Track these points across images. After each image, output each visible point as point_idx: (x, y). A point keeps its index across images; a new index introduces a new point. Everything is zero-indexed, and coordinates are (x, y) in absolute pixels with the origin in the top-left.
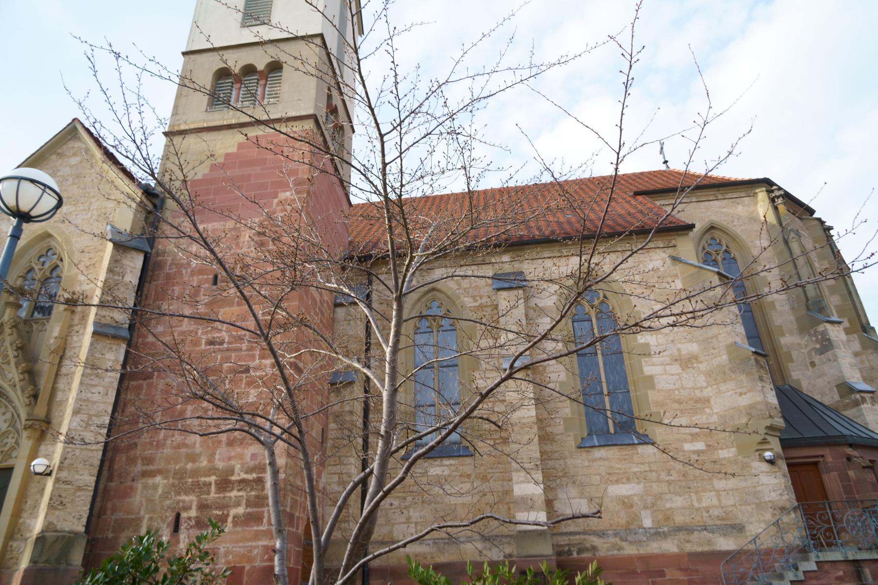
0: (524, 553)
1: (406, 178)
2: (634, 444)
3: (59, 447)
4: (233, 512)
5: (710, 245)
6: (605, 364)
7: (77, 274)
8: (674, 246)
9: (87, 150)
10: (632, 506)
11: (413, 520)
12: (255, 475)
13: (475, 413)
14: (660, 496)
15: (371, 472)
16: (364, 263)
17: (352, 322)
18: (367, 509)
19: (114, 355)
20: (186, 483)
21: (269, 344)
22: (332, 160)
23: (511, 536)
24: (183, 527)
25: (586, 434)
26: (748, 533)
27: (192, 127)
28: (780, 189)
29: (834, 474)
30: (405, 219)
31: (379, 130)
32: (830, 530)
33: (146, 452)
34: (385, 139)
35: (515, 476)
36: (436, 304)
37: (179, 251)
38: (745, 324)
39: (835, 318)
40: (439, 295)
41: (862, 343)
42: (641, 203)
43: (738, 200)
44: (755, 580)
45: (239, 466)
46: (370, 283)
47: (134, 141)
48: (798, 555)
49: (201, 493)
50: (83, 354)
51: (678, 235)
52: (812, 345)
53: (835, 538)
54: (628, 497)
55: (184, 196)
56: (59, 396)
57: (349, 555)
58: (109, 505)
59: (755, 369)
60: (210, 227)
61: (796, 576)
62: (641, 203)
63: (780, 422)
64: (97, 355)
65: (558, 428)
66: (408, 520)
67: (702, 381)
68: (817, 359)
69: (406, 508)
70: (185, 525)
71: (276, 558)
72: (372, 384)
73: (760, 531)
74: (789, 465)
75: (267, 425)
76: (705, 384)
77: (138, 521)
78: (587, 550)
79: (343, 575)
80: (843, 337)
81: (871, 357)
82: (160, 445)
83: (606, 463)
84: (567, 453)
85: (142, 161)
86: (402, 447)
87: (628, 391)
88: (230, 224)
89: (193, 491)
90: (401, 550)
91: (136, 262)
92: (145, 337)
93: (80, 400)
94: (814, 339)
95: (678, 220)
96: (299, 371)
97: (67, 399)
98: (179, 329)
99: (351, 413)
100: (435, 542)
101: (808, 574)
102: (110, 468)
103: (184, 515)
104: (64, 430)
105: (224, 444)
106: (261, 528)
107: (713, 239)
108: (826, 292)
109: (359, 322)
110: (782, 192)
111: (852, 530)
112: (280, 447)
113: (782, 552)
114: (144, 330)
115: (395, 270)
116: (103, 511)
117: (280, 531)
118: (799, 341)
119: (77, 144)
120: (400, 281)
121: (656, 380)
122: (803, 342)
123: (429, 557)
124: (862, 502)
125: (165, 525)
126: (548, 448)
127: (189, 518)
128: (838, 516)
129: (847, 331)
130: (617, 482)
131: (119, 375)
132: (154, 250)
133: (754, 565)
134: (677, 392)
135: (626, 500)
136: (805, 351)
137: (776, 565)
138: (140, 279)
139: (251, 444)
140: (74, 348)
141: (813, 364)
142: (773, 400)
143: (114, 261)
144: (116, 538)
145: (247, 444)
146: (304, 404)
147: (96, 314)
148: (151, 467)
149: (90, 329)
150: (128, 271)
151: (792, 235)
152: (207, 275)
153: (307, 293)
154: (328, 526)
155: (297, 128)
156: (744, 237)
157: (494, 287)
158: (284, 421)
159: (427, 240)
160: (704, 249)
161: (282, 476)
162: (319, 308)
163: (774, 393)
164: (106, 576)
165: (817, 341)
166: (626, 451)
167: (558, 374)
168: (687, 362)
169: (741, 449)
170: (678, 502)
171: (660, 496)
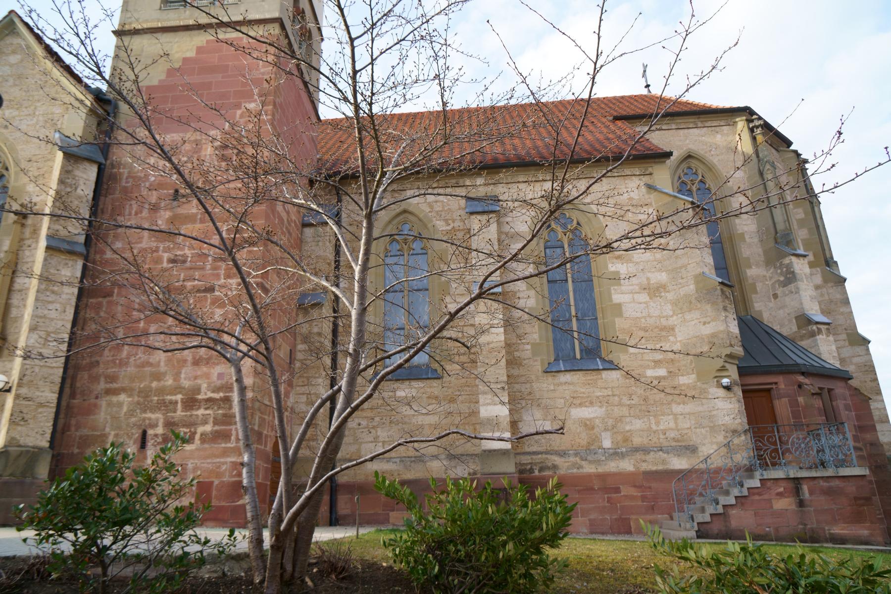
0: (486, 471)
1: (377, 86)
2: (598, 370)
3: (18, 361)
4: (200, 429)
5: (686, 174)
6: (575, 291)
7: (25, 185)
8: (651, 174)
9: (28, 47)
10: (593, 428)
11: (381, 439)
12: (222, 394)
13: (445, 333)
14: (619, 420)
15: (339, 390)
16: (335, 182)
17: (320, 244)
18: (335, 424)
19: (72, 270)
20: (151, 401)
21: (234, 259)
22: (298, 66)
23: (476, 455)
24: (150, 444)
25: (553, 359)
26: (701, 454)
27: (145, 26)
28: (760, 118)
29: (785, 400)
30: (375, 130)
31: (349, 33)
32: (776, 450)
33: (109, 371)
34: (356, 43)
35: (482, 399)
36: (407, 227)
37: (134, 160)
38: (714, 255)
39: (801, 251)
40: (411, 217)
41: (823, 276)
42: (620, 128)
43: (718, 129)
44: (703, 496)
45: (205, 385)
46: (339, 200)
47: (77, 35)
48: (745, 474)
49: (168, 411)
50: (38, 268)
51: (655, 163)
52: (776, 278)
53: (779, 459)
54: (590, 420)
55: (137, 101)
56: (14, 312)
57: (317, 468)
58: (73, 422)
59: (720, 299)
60: (169, 138)
61: (741, 492)
62: (620, 128)
63: (739, 350)
64: (52, 271)
65: (526, 351)
66: (376, 440)
67: (668, 309)
68: (780, 291)
69: (374, 427)
70: (152, 441)
71: (244, 471)
72: (341, 305)
73: (712, 451)
74: (743, 391)
75: (233, 342)
76: (671, 313)
77: (105, 436)
78: (548, 468)
79: (311, 487)
80: (807, 270)
81: (831, 291)
82: (123, 363)
83: (571, 387)
84: (533, 377)
85: (88, 58)
86: (371, 366)
87: (596, 319)
88: (190, 135)
89: (160, 410)
90: (369, 465)
91: (88, 175)
92: (104, 253)
93: (37, 316)
94: (779, 271)
95: (657, 147)
96: (266, 291)
97: (23, 316)
98: (139, 245)
99: (319, 334)
100: (402, 460)
101: (751, 491)
102: (72, 386)
103: (150, 432)
104: (22, 343)
105: (189, 364)
106: (229, 445)
107: (689, 168)
108: (795, 226)
109: (328, 244)
110: (761, 122)
111: (796, 451)
112: (247, 364)
113: (731, 470)
114: (101, 245)
115: (365, 186)
116: (66, 427)
117: (247, 446)
118: (765, 273)
119: (16, 41)
120: (370, 201)
121: (623, 308)
122: (768, 275)
123: (396, 474)
124: (808, 426)
125: (132, 442)
126: (515, 372)
127: (156, 435)
128: (784, 439)
129: (811, 265)
130: (581, 405)
131: (76, 291)
132: (108, 162)
133: (704, 483)
134: (643, 320)
135: (588, 423)
136: (769, 283)
137: (724, 482)
138: (95, 191)
139: (218, 364)
140: (27, 263)
141: (775, 296)
142: (734, 329)
143: (65, 172)
144: (82, 453)
145: (214, 363)
146: (272, 324)
147: (49, 228)
148: (115, 385)
149: (43, 243)
150: (81, 182)
151: (768, 166)
152: (167, 189)
153: (273, 210)
154: (296, 441)
155: (258, 31)
156: (720, 167)
157: (467, 210)
158: (252, 339)
159: (399, 156)
160: (680, 178)
161: (250, 395)
162: (287, 228)
163: (736, 322)
164: (71, 485)
165: (781, 274)
166: (591, 376)
167: (529, 297)
168: (654, 291)
169: (700, 376)
170: (638, 424)
171: (619, 420)
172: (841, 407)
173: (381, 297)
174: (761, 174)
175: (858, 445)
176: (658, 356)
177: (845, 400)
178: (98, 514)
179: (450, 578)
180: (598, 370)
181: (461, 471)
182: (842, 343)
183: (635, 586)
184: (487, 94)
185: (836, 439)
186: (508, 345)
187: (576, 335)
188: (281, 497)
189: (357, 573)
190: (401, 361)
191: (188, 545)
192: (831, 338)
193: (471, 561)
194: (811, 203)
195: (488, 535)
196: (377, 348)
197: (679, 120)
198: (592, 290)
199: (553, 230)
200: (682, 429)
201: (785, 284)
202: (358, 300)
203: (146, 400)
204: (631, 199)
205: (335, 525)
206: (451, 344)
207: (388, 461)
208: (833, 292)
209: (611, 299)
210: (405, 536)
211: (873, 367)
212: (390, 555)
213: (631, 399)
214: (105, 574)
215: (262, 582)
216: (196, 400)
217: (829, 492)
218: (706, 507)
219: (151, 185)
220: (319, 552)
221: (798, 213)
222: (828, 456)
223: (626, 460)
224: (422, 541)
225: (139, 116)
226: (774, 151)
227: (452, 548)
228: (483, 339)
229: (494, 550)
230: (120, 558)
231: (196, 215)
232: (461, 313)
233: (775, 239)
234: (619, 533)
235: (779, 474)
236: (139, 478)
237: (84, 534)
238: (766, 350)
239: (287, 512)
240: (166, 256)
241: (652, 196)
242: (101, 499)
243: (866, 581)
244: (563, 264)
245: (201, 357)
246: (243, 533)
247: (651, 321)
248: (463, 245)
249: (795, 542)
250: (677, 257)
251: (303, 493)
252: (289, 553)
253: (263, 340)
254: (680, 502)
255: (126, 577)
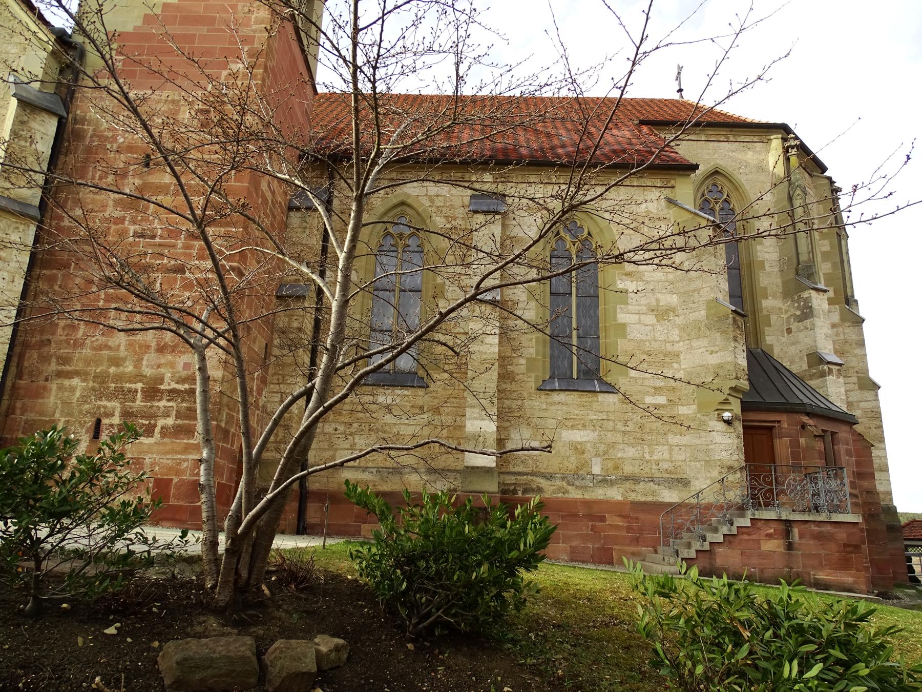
2: (595, 392)
4: (161, 422)
8: (673, 187)
10: (583, 453)
12: (187, 386)
14: (612, 446)
16: (327, 164)
17: (307, 231)
20: (108, 388)
25: (548, 377)
26: (693, 488)
28: (797, 138)
29: (786, 440)
32: (771, 491)
35: (469, 412)
37: (97, 111)
38: (730, 280)
39: (821, 286)
40: (408, 210)
42: (645, 134)
45: (169, 375)
51: (679, 175)
52: (792, 311)
53: (773, 499)
57: (281, 469)
58: (19, 404)
62: (645, 134)
63: (744, 384)
65: (520, 365)
67: (675, 335)
68: (794, 326)
69: (351, 434)
70: (107, 432)
73: (705, 486)
74: (744, 427)
75: (199, 327)
78: (533, 490)
79: (274, 489)
80: (826, 306)
81: (847, 330)
83: (564, 407)
84: (525, 394)
86: (349, 364)
87: (598, 338)
91: (45, 129)
92: (61, 218)
94: (796, 305)
102: (19, 365)
103: (105, 421)
105: (152, 350)
106: (192, 441)
107: (715, 185)
108: (819, 258)
111: (791, 493)
118: (781, 305)
122: (784, 307)
125: (84, 431)
126: (508, 387)
127: (112, 425)
129: (831, 302)
133: (692, 518)
134: (647, 343)
135: (579, 446)
136: (784, 316)
138: (54, 148)
139: (184, 353)
141: (789, 331)
142: (743, 362)
143: (19, 122)
145: (180, 352)
148: (68, 368)
151: (798, 191)
153: (257, 187)
156: (747, 188)
157: (471, 208)
158: (222, 326)
160: (703, 195)
162: (271, 210)
165: (798, 308)
166: (586, 398)
167: (529, 306)
168: (663, 313)
169: (701, 407)
170: (631, 452)
171: (612, 446)
172: (843, 452)
173: (366, 289)
174: (790, 199)
175: (854, 491)
176: (660, 383)
177: (848, 445)
178: (32, 502)
179: (418, 596)
180: (595, 392)
181: (440, 486)
182: (852, 386)
183: (612, 617)
184: (506, 78)
185: (833, 484)
186: (502, 358)
187: (574, 348)
188: (241, 498)
189: (320, 584)
190: (383, 360)
191: (133, 544)
192: (841, 380)
193: (441, 580)
194: (839, 235)
195: (461, 553)
196: (357, 346)
197: (710, 131)
198: (597, 306)
199: (561, 238)
200: (676, 461)
201: (800, 319)
202: (340, 291)
203: (102, 387)
204: (648, 212)
205: (303, 534)
206: (440, 349)
207: (364, 471)
208: (850, 333)
209: (615, 319)
210: (374, 550)
211: (880, 413)
212: (357, 567)
213: (626, 425)
214: (38, 568)
215: (214, 587)
216: (158, 391)
217: (819, 537)
218: (693, 543)
219: (118, 147)
220: (280, 560)
221: (824, 245)
222: (822, 501)
223: (615, 488)
224: (391, 555)
225: (101, 53)
226: (806, 175)
227: (422, 564)
228: (474, 347)
229: (467, 569)
230: (56, 552)
231: (168, 186)
232: (453, 314)
233: (797, 270)
234: (600, 563)
235: (770, 514)
236: (82, 467)
237: (14, 524)
238: (772, 386)
239: (246, 514)
240: (132, 228)
241: (671, 211)
242: (36, 487)
243: (848, 626)
244: (569, 271)
245: (166, 343)
246: (197, 536)
247: (656, 345)
248: (464, 243)
249: (780, 584)
250: (690, 280)
251: (265, 495)
252: (245, 558)
253: (233, 327)
254: (666, 535)
255: (63, 574)
